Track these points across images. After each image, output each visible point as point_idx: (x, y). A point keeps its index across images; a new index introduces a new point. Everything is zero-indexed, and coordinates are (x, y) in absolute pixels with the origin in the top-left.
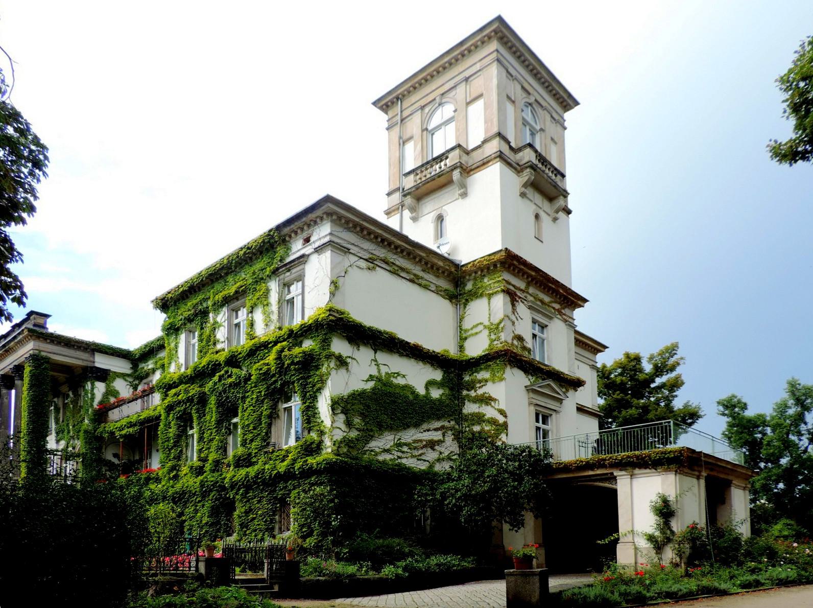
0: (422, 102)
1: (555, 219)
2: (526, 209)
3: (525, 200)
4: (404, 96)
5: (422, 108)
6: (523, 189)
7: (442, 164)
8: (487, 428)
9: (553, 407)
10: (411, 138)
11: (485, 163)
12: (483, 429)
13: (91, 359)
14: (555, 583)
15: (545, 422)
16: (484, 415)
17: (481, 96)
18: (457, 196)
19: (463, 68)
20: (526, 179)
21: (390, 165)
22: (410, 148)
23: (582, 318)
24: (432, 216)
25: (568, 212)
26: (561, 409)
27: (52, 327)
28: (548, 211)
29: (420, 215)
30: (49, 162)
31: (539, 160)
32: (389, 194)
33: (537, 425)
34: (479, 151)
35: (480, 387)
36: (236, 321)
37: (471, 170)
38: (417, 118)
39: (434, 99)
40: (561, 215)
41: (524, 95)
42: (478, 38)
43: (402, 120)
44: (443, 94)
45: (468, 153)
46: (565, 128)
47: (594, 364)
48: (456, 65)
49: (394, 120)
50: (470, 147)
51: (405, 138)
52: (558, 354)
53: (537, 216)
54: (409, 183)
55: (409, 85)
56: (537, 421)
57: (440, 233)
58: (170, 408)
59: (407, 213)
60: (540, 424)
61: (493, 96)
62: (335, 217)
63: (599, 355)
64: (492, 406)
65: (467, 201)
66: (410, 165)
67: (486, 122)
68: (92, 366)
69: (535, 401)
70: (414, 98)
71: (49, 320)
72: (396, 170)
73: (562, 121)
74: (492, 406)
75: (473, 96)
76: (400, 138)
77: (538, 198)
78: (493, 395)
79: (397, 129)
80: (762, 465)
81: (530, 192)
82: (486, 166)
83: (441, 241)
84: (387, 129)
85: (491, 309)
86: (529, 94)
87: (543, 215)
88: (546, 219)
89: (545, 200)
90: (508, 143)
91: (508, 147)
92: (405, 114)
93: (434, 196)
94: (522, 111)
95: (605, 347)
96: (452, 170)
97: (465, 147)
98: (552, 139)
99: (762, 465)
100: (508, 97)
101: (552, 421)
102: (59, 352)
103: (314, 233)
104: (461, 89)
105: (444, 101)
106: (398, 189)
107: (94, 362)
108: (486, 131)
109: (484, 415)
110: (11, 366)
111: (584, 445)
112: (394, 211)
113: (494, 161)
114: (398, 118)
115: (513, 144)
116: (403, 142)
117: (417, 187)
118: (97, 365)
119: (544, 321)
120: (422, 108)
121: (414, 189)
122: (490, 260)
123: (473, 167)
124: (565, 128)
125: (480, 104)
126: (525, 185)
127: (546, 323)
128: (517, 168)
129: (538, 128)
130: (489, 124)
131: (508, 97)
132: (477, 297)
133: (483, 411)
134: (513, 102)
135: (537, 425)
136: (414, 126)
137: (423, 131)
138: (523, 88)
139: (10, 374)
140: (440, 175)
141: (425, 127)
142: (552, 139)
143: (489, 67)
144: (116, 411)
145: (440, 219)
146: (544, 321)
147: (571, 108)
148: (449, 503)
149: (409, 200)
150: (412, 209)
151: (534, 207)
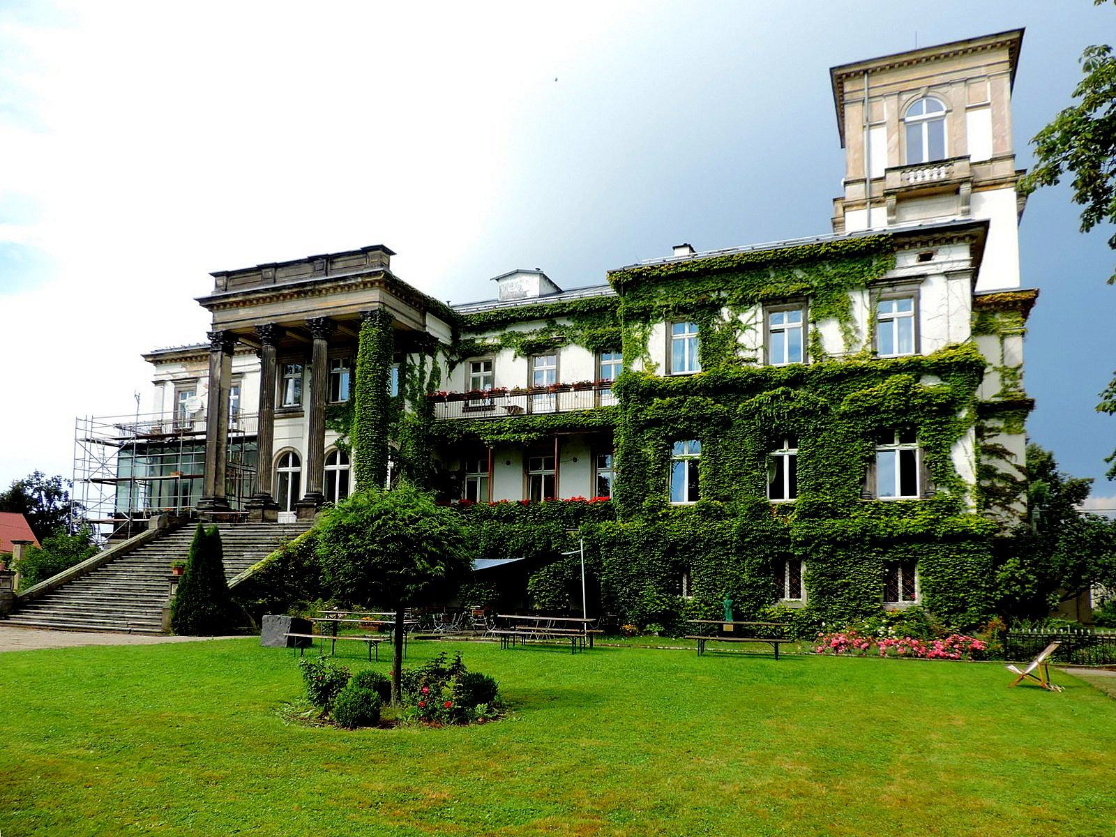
5: (900, 93)
8: (1000, 485)
11: (996, 184)
12: (993, 485)
16: (996, 469)
19: (960, 67)
27: (399, 269)
35: (989, 437)
42: (992, 41)
55: (887, 63)
64: (1007, 461)
67: (994, 137)
70: (887, 79)
74: (1007, 461)
78: (1009, 449)
80: (1063, 522)
82: (997, 187)
85: (1005, 350)
93: (919, 203)
96: (961, 183)
99: (1063, 522)
103: (940, 252)
105: (930, 94)
109: (996, 469)
113: (1009, 185)
120: (900, 93)
121: (904, 190)
122: (1013, 297)
123: (980, 184)
130: (1000, 141)
132: (986, 333)
133: (994, 465)
137: (900, 120)
143: (998, 77)
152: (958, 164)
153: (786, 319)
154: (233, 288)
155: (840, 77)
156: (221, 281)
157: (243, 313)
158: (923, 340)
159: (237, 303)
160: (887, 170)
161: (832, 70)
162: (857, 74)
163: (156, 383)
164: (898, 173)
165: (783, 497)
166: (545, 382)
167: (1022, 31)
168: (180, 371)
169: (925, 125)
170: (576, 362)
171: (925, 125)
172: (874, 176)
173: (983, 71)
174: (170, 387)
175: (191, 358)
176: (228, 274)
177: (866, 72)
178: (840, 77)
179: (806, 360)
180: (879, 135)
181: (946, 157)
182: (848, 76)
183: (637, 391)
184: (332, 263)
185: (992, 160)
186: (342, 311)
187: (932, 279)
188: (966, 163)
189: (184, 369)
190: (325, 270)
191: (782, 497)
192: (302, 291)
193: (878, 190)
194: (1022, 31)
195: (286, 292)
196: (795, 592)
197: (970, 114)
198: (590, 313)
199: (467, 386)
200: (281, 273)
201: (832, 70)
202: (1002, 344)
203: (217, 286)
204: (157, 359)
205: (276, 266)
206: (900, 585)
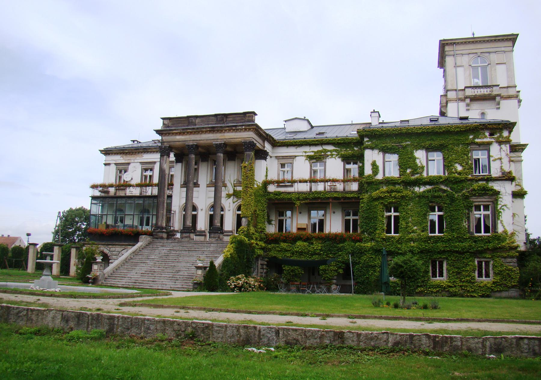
42: (506, 38)
152: (494, 88)
153: (435, 156)
154: (172, 125)
155: (444, 44)
156: (166, 122)
157: (178, 138)
158: (491, 168)
159: (176, 133)
160: (466, 87)
161: (440, 41)
162: (451, 43)
163: (105, 164)
164: (470, 89)
165: (435, 233)
166: (319, 176)
167: (517, 35)
168: (119, 159)
169: (479, 69)
170: (334, 167)
171: (479, 69)
172: (459, 88)
173: (503, 49)
174: (113, 168)
175: (127, 153)
176: (170, 119)
177: (454, 43)
178: (443, 45)
179: (444, 173)
180: (460, 70)
181: (489, 85)
182: (447, 44)
183: (367, 184)
184: (226, 117)
185: (508, 87)
186: (233, 141)
187: (297, 158)
188: (498, 88)
189: (122, 158)
190: (222, 121)
191: (435, 233)
192: (213, 130)
193: (461, 95)
194: (517, 35)
195: (204, 130)
196: (441, 275)
197: (498, 66)
198: (341, 143)
199: (279, 175)
200: (198, 120)
201: (440, 41)
202: (498, 159)
203: (164, 124)
204: (107, 152)
205: (197, 117)
206: (484, 271)
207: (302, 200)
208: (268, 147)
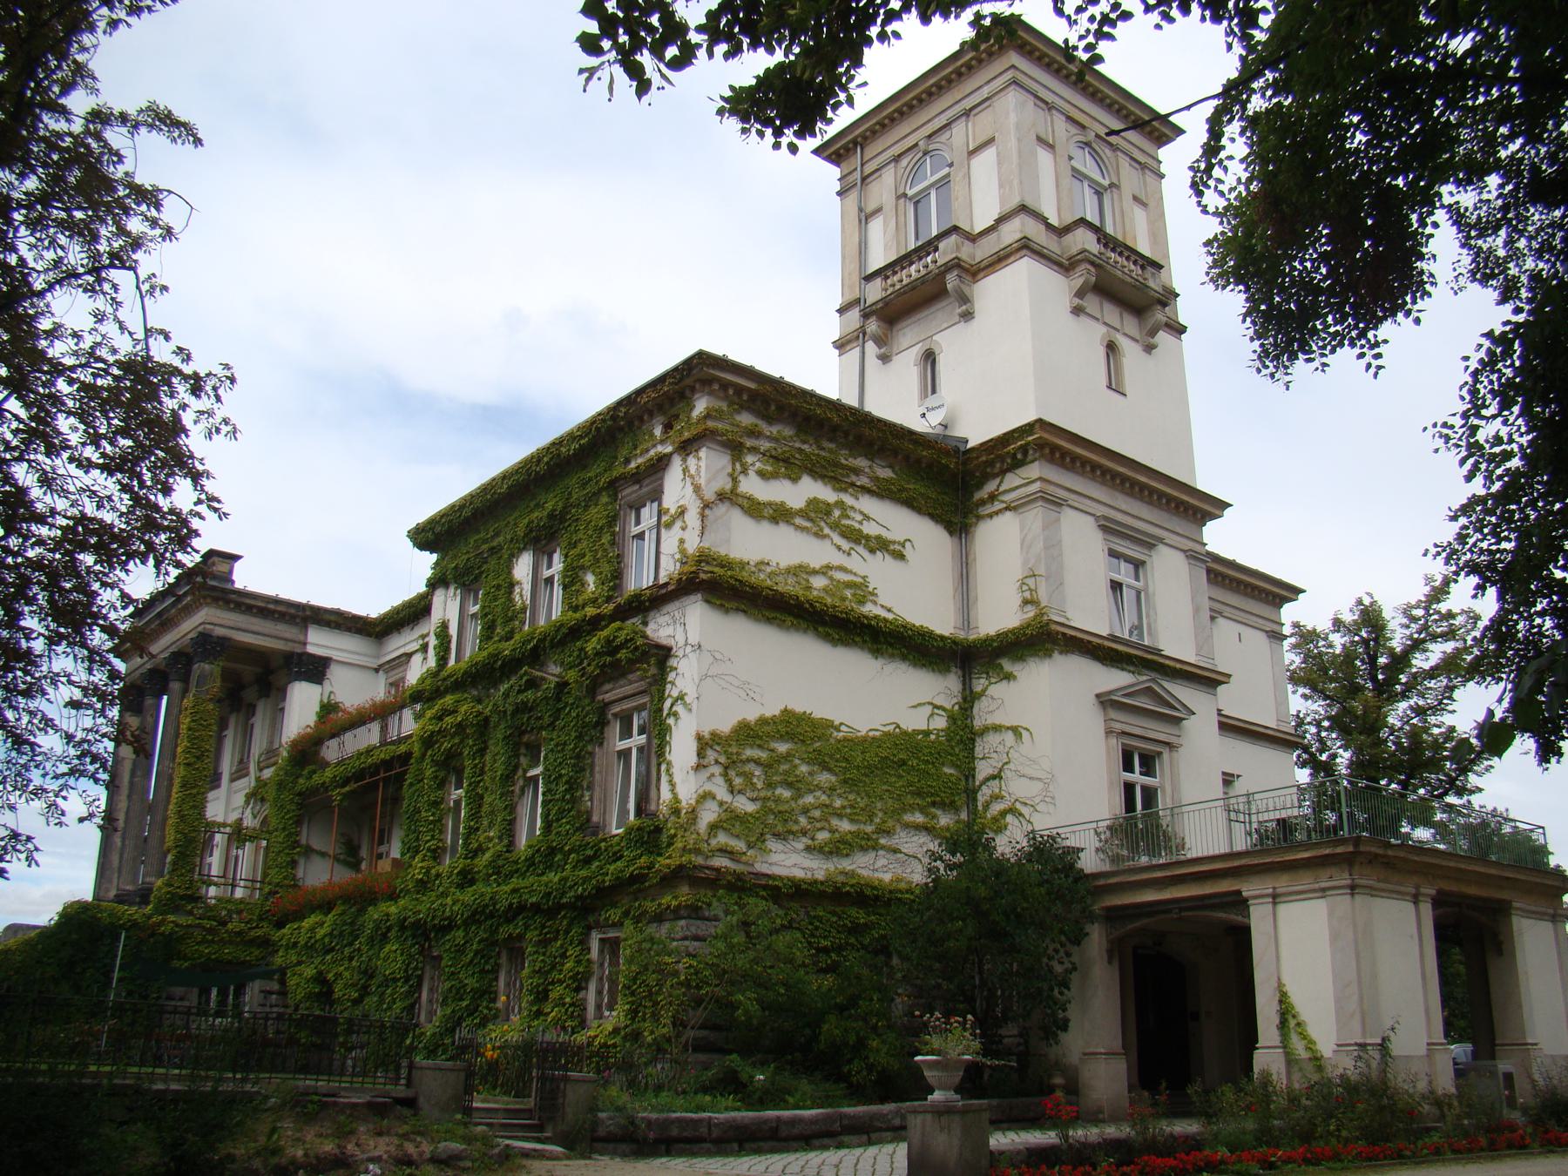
0: (897, 150)
1: (1149, 348)
2: (1086, 337)
3: (1083, 318)
4: (865, 138)
5: (897, 159)
6: (1077, 301)
7: (929, 259)
9: (1162, 737)
10: (878, 210)
11: (1000, 259)
13: (301, 638)
14: (1001, 1140)
15: (1148, 769)
17: (990, 141)
18: (957, 318)
20: (1080, 281)
21: (843, 257)
22: (876, 227)
23: (1218, 537)
24: (914, 353)
25: (1180, 330)
26: (1181, 741)
27: (245, 578)
28: (1134, 332)
29: (895, 350)
30: (219, 501)
31: (1105, 246)
32: (841, 311)
33: (1128, 776)
34: (993, 236)
36: (547, 573)
37: (980, 270)
38: (888, 176)
39: (916, 145)
40: (1163, 337)
41: (1074, 130)
43: (864, 179)
44: (930, 136)
45: (973, 238)
46: (1162, 176)
47: (1275, 627)
48: (949, 89)
49: (851, 178)
50: (978, 229)
51: (869, 209)
52: (1175, 620)
53: (1111, 347)
54: (875, 292)
56: (1128, 767)
57: (930, 384)
58: (428, 741)
59: (871, 347)
60: (1136, 777)
61: (1010, 142)
62: (716, 387)
63: (1286, 606)
65: (974, 323)
66: (877, 261)
67: (1001, 186)
68: (299, 651)
69: (1118, 727)
71: (238, 565)
72: (854, 266)
73: (1154, 164)
75: (980, 141)
76: (861, 210)
77: (1111, 313)
79: (853, 196)
81: (1092, 303)
83: (932, 401)
84: (839, 194)
86: (1083, 127)
87: (1124, 343)
88: (1130, 351)
89: (1125, 315)
90: (1045, 221)
91: (1042, 227)
92: (868, 169)
94: (1071, 158)
95: (1300, 591)
97: (967, 229)
98: (1135, 198)
100: (1040, 140)
101: (1162, 769)
102: (243, 626)
104: (958, 130)
106: (857, 301)
107: (305, 644)
108: (1002, 201)
110: (166, 655)
111: (1241, 818)
112: (849, 342)
114: (857, 175)
115: (1054, 221)
116: (865, 217)
117: (886, 302)
118: (311, 649)
119: (1135, 552)
124: (1162, 176)
125: (989, 154)
126: (1080, 294)
127: (1143, 558)
128: (1065, 266)
129: (1106, 183)
131: (1040, 140)
134: (1051, 147)
135: (1128, 776)
136: (883, 189)
137: (898, 198)
138: (1070, 119)
139: (162, 667)
140: (922, 281)
141: (901, 191)
142: (1135, 198)
144: (333, 743)
145: (930, 358)
146: (1135, 552)
147: (1169, 140)
148: (179, 1078)
149: (873, 326)
150: (880, 341)
151: (1104, 329)
207: (343, 786)
208: (319, 642)
